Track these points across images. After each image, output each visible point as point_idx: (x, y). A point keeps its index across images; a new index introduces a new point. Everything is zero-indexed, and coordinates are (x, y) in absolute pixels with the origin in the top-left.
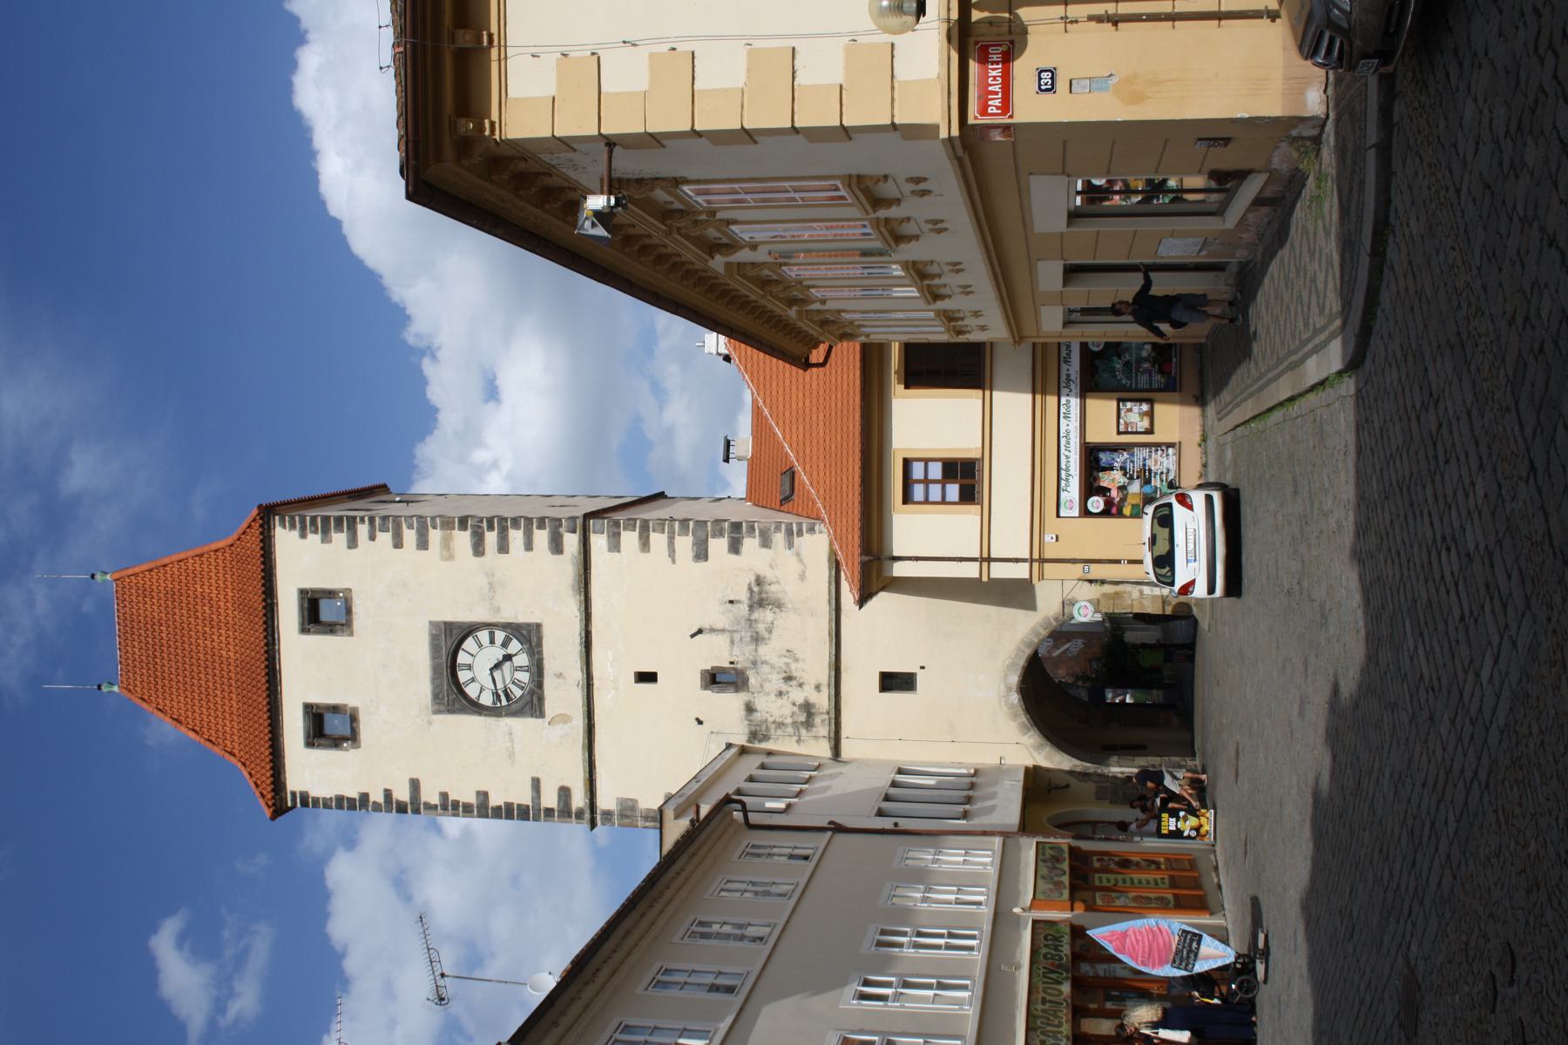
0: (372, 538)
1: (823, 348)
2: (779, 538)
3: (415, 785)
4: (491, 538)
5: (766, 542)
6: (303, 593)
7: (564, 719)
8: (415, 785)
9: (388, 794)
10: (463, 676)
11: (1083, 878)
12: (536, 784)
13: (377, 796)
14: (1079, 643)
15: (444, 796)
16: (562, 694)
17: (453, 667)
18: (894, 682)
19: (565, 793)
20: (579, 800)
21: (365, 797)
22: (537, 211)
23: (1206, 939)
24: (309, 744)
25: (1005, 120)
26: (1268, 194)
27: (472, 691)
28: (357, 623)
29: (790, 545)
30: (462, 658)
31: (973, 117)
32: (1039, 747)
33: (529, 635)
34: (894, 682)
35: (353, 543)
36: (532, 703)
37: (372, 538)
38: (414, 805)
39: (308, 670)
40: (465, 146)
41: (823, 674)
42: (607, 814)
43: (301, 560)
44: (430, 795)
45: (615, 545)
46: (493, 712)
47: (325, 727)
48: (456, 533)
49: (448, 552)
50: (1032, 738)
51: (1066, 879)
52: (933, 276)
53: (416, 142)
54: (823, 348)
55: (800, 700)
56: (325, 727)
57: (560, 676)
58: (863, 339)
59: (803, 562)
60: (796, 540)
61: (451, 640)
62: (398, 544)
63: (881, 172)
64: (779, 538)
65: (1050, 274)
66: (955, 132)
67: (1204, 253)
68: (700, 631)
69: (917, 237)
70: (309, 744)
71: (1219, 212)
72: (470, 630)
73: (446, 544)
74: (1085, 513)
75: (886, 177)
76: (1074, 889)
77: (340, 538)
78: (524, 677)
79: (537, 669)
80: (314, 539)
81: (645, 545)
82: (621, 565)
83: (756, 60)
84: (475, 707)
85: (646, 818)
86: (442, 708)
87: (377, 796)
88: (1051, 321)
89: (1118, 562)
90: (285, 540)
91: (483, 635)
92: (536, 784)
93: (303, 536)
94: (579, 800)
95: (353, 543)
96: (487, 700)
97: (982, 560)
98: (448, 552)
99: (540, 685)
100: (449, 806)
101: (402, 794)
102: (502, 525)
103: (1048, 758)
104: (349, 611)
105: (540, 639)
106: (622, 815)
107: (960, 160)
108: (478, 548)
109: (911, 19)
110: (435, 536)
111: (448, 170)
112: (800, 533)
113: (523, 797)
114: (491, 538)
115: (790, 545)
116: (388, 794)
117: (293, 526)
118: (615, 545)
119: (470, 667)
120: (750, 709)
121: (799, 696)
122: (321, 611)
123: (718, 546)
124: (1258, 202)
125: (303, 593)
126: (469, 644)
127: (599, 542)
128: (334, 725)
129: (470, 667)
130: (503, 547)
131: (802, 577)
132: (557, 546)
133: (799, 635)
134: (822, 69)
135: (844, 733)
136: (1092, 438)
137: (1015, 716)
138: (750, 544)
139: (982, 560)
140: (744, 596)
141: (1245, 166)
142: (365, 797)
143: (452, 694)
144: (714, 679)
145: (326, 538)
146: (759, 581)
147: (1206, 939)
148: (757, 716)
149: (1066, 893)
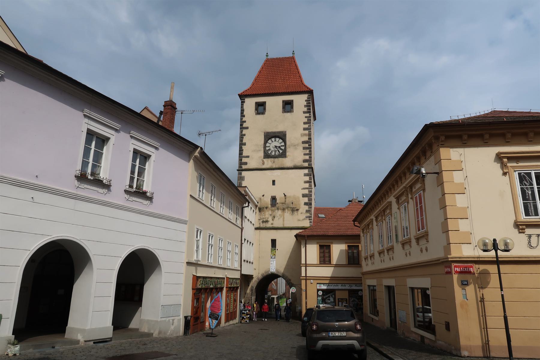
0: (306, 117)
1: (358, 225)
2: (308, 215)
3: (247, 128)
4: (307, 145)
5: (307, 211)
6: (292, 101)
7: (263, 164)
8: (247, 128)
9: (245, 122)
10: (273, 139)
11: (232, 290)
12: (248, 157)
13: (244, 119)
14: (275, 288)
15: (245, 135)
16: (268, 163)
17: (275, 137)
18: (274, 242)
19: (246, 163)
20: (244, 167)
21: (244, 116)
22: (415, 155)
23: (217, 322)
24: (283, 101)
25: (453, 272)
26: (426, 340)
27: (270, 141)
28: (258, 116)
30: (277, 139)
31: (453, 265)
32: (258, 278)
33: (283, 155)
34: (274, 242)
35: (304, 112)
36: (267, 156)
37: (306, 117)
38: (242, 128)
39: (274, 103)
40: (437, 138)
41: (276, 225)
42: (241, 174)
43: (299, 101)
44: (244, 132)
45: (305, 175)
46: (265, 147)
47: (260, 108)
49: (303, 135)
50: (260, 277)
51: (232, 286)
52: (388, 252)
53: (490, 124)
54: (358, 225)
55: (269, 220)
56: (260, 108)
57: (274, 162)
58: (362, 235)
59: (301, 219)
61: (282, 136)
62: (305, 123)
63: (429, 240)
64: (308, 215)
65: (391, 282)
66: (450, 259)
67: (400, 322)
68: (285, 196)
69: (404, 249)
70: (283, 101)
71: (415, 327)
72: (284, 141)
73: (305, 135)
74: (318, 290)
75: (428, 241)
76: (230, 288)
77: (305, 109)
78: (273, 154)
79: (275, 157)
80: (305, 103)
81: (306, 182)
82: (300, 176)
83: (465, 209)
84: (266, 142)
85: (240, 183)
87: (244, 119)
88: (371, 282)
90: (305, 97)
91: (283, 144)
92: (248, 157)
93: (306, 101)
94: (244, 167)
95: (304, 112)
96: (268, 145)
97: (306, 264)
98: (303, 135)
99: (271, 157)
100: (242, 136)
101: (245, 125)
102: (310, 148)
103: (255, 281)
104: (288, 112)
105: (283, 157)
106: (240, 177)
107: (439, 260)
108: (304, 142)
109: (482, 248)
110: (307, 132)
111: (431, 134)
112: (309, 220)
113: (245, 154)
114: (307, 145)
116: (245, 122)
117: (308, 98)
118: (305, 175)
119: (275, 141)
120: (267, 208)
121: (270, 219)
122: (288, 106)
123: (306, 200)
124: (422, 337)
125: (292, 101)
126: (281, 141)
127: (306, 171)
128: (261, 108)
129: (275, 141)
130: (304, 148)
131: (299, 220)
132: (305, 161)
133: (290, 220)
134: (463, 226)
135: (261, 231)
136: (337, 292)
137: (266, 272)
138: (307, 208)
139: (306, 264)
140: (293, 206)
141: (437, 334)
142: (244, 116)
143: (269, 136)
144: (274, 199)
145: (305, 106)
146: (297, 210)
147: (217, 322)
148: (265, 209)
149: (230, 286)
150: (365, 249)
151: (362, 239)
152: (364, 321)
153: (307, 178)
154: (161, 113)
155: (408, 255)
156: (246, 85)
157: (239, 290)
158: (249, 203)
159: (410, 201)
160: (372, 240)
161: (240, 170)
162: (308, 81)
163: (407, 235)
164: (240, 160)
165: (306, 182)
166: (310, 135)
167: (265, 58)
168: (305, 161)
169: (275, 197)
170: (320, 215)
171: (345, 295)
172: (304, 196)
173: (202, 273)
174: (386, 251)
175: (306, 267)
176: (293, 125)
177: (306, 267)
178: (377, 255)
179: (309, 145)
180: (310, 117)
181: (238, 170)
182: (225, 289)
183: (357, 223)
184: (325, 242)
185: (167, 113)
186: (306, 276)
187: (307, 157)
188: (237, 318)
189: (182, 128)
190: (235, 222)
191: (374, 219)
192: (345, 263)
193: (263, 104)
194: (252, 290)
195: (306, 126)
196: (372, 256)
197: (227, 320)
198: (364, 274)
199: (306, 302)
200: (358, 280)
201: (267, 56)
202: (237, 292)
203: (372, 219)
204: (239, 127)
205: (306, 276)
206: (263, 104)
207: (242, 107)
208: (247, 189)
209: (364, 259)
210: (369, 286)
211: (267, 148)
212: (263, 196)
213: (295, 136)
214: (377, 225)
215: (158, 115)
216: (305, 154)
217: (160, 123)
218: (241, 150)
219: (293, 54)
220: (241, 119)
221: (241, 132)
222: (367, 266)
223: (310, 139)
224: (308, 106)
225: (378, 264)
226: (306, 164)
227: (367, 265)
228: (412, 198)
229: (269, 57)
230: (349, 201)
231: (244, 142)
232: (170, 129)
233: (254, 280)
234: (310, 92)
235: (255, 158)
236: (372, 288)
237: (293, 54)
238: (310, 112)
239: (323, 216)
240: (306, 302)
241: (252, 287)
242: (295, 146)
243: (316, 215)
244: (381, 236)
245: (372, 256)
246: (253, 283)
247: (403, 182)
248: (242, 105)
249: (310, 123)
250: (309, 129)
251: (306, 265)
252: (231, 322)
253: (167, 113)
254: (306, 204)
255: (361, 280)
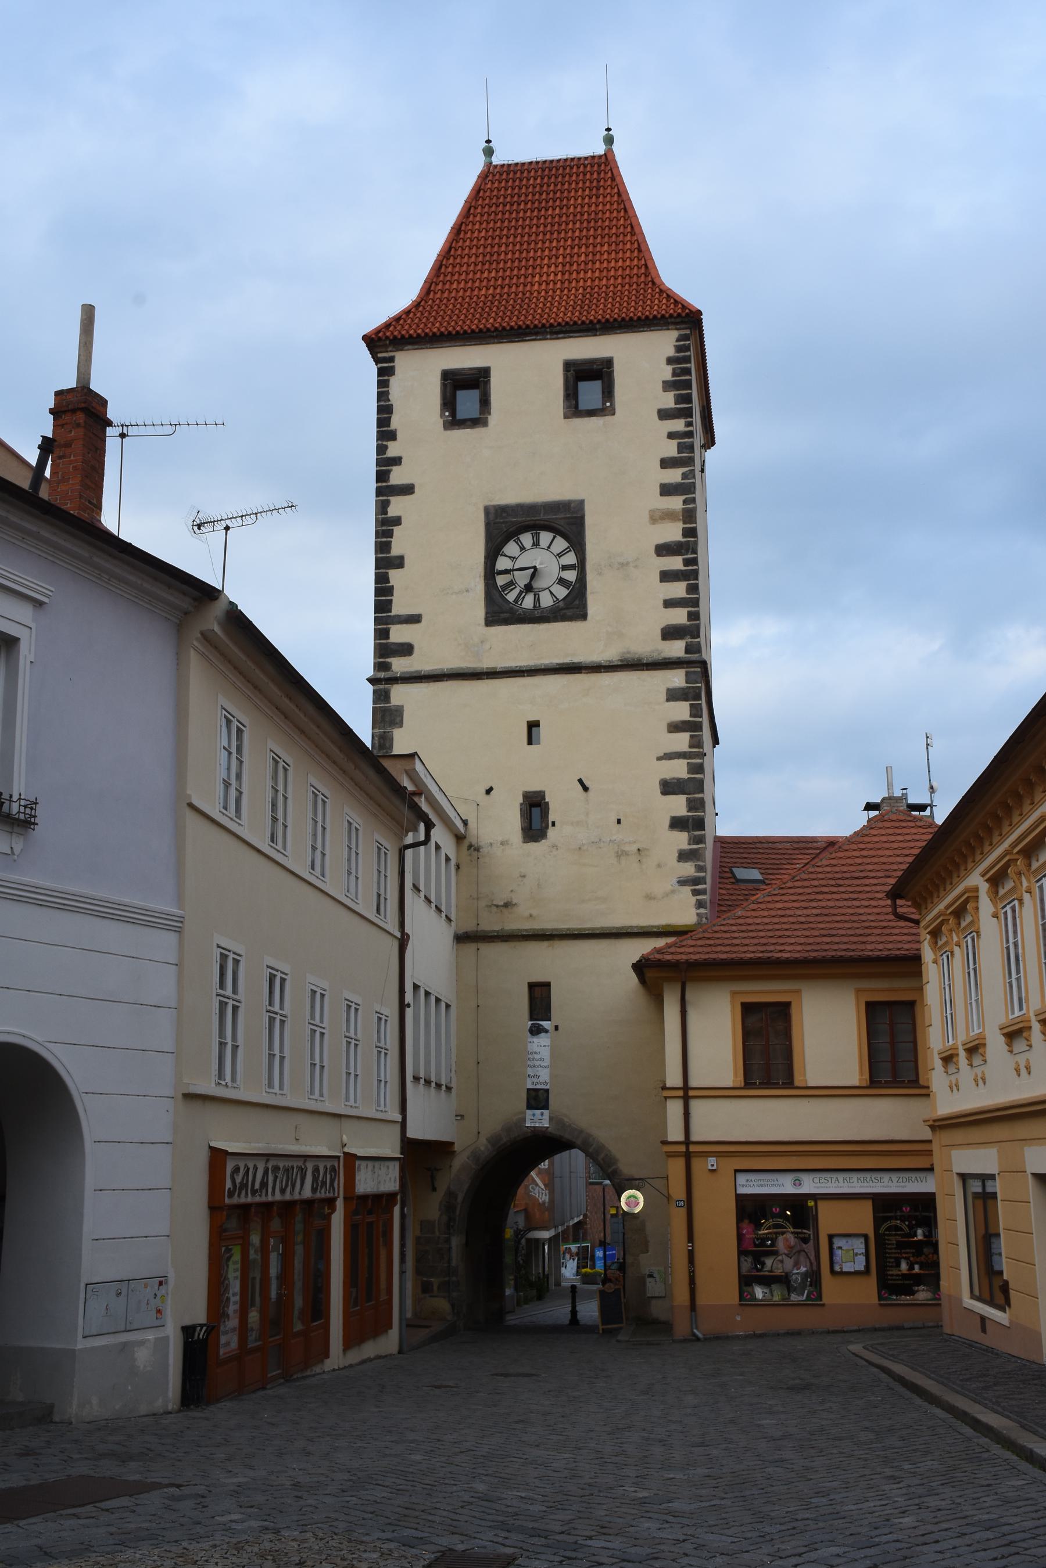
0: (671, 436)
2: (688, 869)
3: (407, 490)
4: (676, 563)
5: (684, 856)
6: (609, 363)
8: (407, 490)
9: (397, 461)
10: (527, 539)
13: (393, 449)
15: (397, 521)
17: (535, 528)
18: (540, 998)
20: (399, 665)
21: (392, 436)
27: (511, 548)
29: (683, 882)
30: (545, 537)
33: (573, 607)
35: (664, 415)
36: (500, 612)
37: (671, 436)
39: (526, 373)
43: (641, 361)
44: (397, 506)
45: (673, 695)
46: (490, 572)
47: (465, 398)
48: (680, 526)
52: (969, 1059)
56: (465, 398)
60: (687, 890)
61: (566, 522)
62: (666, 463)
64: (688, 869)
72: (576, 541)
73: (668, 516)
75: (1030, 1046)
77: (669, 401)
80: (667, 373)
81: (675, 727)
82: (650, 695)
84: (493, 552)
86: (492, 517)
87: (393, 449)
88: (976, 1158)
89: (691, 1238)
90: (664, 343)
91: (571, 559)
93: (670, 361)
95: (664, 415)
96: (502, 563)
101: (397, 476)
104: (591, 413)
108: (662, 550)
110: (676, 503)
112: (695, 893)
113: (398, 608)
114: (676, 563)
115: (683, 882)
116: (397, 461)
117: (679, 349)
118: (673, 695)
119: (536, 544)
122: (588, 386)
125: (609, 363)
126: (561, 544)
127: (677, 679)
129: (536, 544)
130: (666, 576)
132: (670, 633)
138: (681, 840)
139: (686, 1087)
142: (392, 436)
143: (505, 526)
145: (667, 386)
150: (968, 1005)
151: (931, 971)
152: (947, 1330)
153: (681, 711)
154: (47, 446)
155: (1023, 1071)
156: (399, 289)
157: (397, 1210)
158: (429, 826)
159: (1026, 897)
160: (974, 974)
161: (383, 681)
162: (677, 272)
163: (1021, 1009)
164: (381, 634)
165: (675, 727)
166: (689, 515)
167: (477, 166)
168: (670, 633)
169: (541, 795)
170: (741, 873)
171: (863, 1218)
172: (669, 787)
173: (237, 1138)
174: (962, 1054)
175: (686, 1099)
176: (611, 468)
177: (686, 1099)
178: (996, 1043)
179: (687, 562)
180: (690, 434)
181: (371, 680)
182: (340, 1204)
183: (904, 907)
184: (766, 991)
185: (68, 445)
186: (687, 1142)
187: (679, 616)
188: (394, 1333)
189: (138, 511)
190: (371, 915)
191: (984, 887)
192: (856, 1082)
193: (477, 380)
194: (448, 1207)
195: (674, 475)
196: (975, 1049)
197: (351, 1341)
198: (941, 1125)
199: (691, 1255)
200: (913, 1154)
201: (489, 152)
202: (391, 1212)
203: (976, 889)
204: (372, 485)
205: (687, 1142)
206: (477, 380)
207: (383, 395)
208: (418, 766)
209: (938, 1063)
210: (964, 1177)
211: (501, 580)
212: (489, 791)
213: (624, 532)
214: (995, 916)
215: (32, 457)
216: (669, 604)
217: (44, 493)
218: (383, 591)
219: (609, 140)
220: (381, 449)
221: (382, 507)
222: (952, 1094)
223: (691, 533)
224: (678, 384)
225: (1001, 1084)
226: (676, 649)
227: (954, 1087)
228: (1029, 892)
229: (496, 160)
230: (869, 807)
231: (395, 551)
232: (85, 516)
233: (457, 1163)
234: (688, 321)
235: (450, 621)
236: (976, 1187)
237: (609, 140)
238: (687, 413)
239: (755, 874)
240: (691, 1255)
241: (450, 1194)
242: (623, 565)
243: (725, 873)
244: (1013, 959)
245: (975, 1049)
246: (457, 1173)
247: (995, 842)
248: (383, 385)
249: (690, 461)
250: (686, 489)
251: (686, 1093)
252: (370, 1349)
253: (68, 445)
254: (677, 824)
255: (930, 1153)
